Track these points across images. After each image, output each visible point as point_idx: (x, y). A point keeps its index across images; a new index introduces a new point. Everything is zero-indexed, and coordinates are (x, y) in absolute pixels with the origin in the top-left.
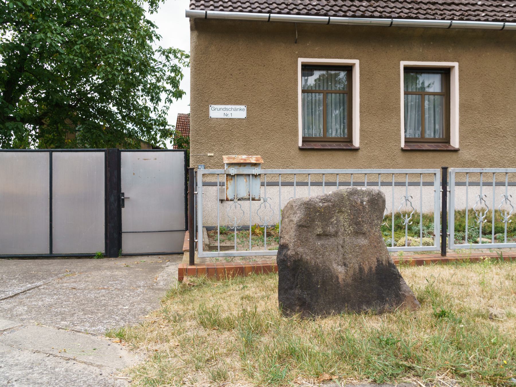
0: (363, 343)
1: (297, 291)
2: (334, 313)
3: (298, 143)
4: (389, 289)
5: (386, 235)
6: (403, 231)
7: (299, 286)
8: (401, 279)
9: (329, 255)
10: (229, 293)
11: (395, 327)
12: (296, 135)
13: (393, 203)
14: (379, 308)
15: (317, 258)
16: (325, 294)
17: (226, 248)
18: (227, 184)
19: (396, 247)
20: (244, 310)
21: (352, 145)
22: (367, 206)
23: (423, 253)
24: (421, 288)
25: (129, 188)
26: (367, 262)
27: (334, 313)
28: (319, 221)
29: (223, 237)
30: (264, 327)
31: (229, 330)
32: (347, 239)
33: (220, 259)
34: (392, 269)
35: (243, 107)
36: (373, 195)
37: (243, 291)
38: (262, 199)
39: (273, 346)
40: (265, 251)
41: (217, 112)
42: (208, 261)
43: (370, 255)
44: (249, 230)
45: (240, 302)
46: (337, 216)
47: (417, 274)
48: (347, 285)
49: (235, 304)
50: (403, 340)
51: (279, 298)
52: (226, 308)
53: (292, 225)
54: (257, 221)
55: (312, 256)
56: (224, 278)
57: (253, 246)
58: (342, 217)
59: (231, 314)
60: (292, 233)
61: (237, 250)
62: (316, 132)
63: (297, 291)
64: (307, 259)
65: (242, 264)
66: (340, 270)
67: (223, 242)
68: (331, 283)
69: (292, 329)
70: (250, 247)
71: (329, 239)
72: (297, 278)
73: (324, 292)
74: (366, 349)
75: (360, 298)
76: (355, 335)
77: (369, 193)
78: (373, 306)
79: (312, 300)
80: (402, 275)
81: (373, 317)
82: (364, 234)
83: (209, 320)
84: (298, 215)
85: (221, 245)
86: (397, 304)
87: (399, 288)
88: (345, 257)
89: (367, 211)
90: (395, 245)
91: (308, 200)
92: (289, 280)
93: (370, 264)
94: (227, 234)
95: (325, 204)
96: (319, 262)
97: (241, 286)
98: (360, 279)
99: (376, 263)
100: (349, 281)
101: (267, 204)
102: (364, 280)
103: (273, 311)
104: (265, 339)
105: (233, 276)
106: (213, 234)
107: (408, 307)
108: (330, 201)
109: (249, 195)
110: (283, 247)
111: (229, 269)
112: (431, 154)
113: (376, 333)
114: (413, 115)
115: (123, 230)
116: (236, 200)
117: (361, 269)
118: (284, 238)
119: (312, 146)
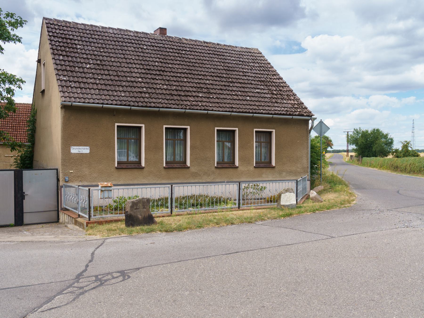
1: (130, 222)
3: (115, 165)
12: (114, 161)
21: (141, 165)
25: (28, 189)
35: (88, 147)
41: (74, 150)
60: (129, 208)
62: (124, 159)
66: (140, 217)
93: (147, 215)
112: (177, 170)
114: (170, 150)
115: (24, 212)
119: (123, 166)
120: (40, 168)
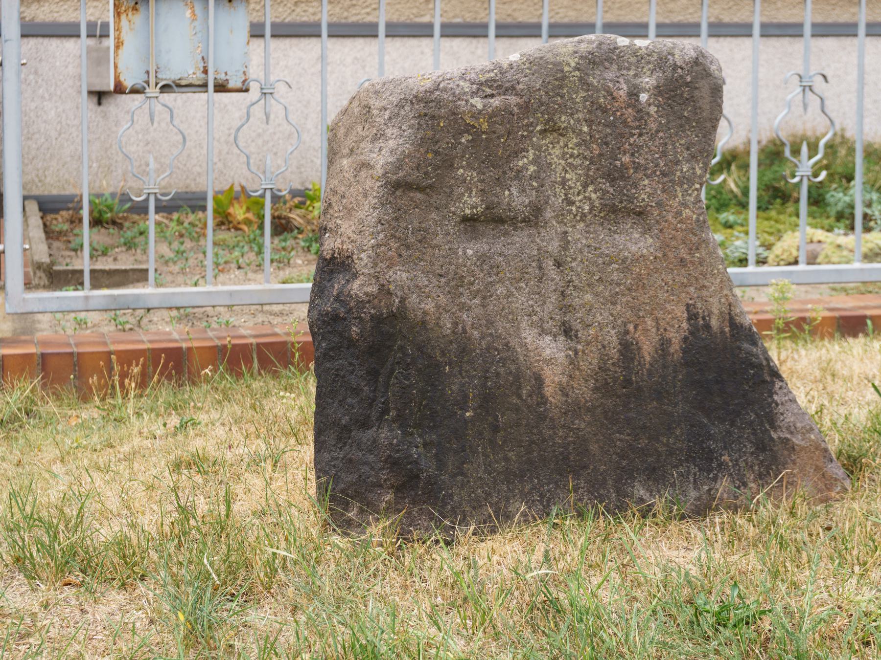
0: (633, 623)
2: (524, 514)
4: (733, 423)
5: (728, 226)
6: (790, 208)
7: (393, 413)
8: (778, 384)
9: (509, 295)
10: (126, 448)
11: (753, 561)
13: (755, 103)
14: (693, 494)
15: (463, 307)
16: (492, 442)
17: (117, 278)
18: (118, 29)
19: (765, 268)
20: (182, 509)
22: (653, 110)
23: (867, 287)
24: (853, 419)
26: (649, 322)
27: (524, 514)
28: (470, 167)
29: (102, 237)
30: (259, 571)
31: (123, 586)
32: (577, 233)
33: (93, 317)
34: (746, 345)
36: (675, 67)
37: (180, 437)
38: (254, 87)
39: (292, 639)
40: (267, 286)
42: (45, 329)
43: (662, 295)
44: (204, 209)
45: (168, 480)
46: (539, 148)
47: (838, 366)
48: (574, 409)
49: (150, 488)
50: (779, 608)
51: (317, 461)
52: (113, 504)
53: (369, 183)
54: (238, 175)
55: (443, 300)
56: (107, 391)
57: (220, 268)
58: (557, 151)
59: (133, 526)
60: (368, 211)
61: (158, 285)
63: (384, 435)
64: (425, 313)
65: (176, 336)
66: (548, 353)
67: (104, 254)
68: (515, 400)
69: (364, 575)
70: (210, 273)
71: (506, 234)
72: (387, 386)
73: (487, 434)
74: (643, 645)
75: (622, 457)
76: (601, 593)
77: (662, 61)
78: (673, 485)
79: (441, 465)
80: (784, 371)
81: (673, 527)
82: (641, 214)
83: (47, 550)
84: (391, 143)
85: (99, 266)
86: (760, 476)
87: (771, 419)
88: (567, 301)
89: (653, 126)
90: (761, 262)
91: (428, 84)
92: (356, 391)
93: (662, 328)
94: (120, 226)
95: (496, 102)
96: (469, 321)
97: (174, 421)
98: (624, 384)
99: (685, 325)
100: (584, 391)
101: (276, 108)
102: (639, 389)
103: (293, 511)
104: (262, 617)
105: (143, 384)
106: (66, 227)
107: (805, 488)
108: (511, 89)
109: (205, 72)
110: (332, 267)
111: (128, 357)
113: (680, 586)
116: (152, 91)
117: (628, 349)
118: (335, 231)
120: (16, 317)
